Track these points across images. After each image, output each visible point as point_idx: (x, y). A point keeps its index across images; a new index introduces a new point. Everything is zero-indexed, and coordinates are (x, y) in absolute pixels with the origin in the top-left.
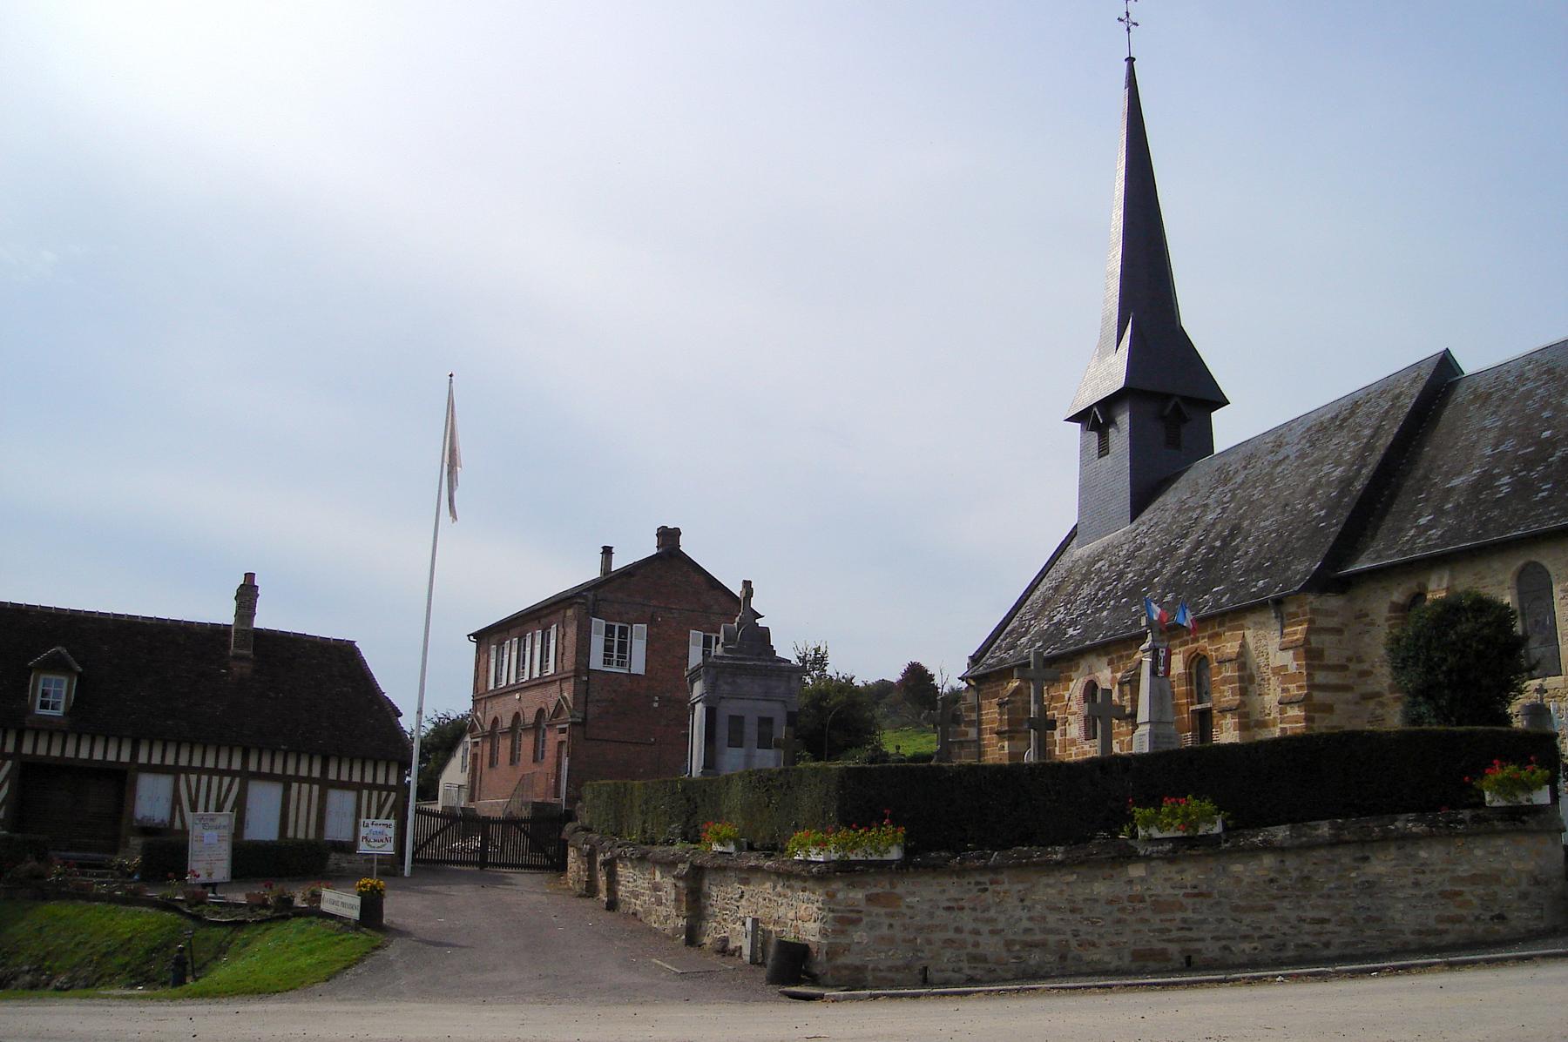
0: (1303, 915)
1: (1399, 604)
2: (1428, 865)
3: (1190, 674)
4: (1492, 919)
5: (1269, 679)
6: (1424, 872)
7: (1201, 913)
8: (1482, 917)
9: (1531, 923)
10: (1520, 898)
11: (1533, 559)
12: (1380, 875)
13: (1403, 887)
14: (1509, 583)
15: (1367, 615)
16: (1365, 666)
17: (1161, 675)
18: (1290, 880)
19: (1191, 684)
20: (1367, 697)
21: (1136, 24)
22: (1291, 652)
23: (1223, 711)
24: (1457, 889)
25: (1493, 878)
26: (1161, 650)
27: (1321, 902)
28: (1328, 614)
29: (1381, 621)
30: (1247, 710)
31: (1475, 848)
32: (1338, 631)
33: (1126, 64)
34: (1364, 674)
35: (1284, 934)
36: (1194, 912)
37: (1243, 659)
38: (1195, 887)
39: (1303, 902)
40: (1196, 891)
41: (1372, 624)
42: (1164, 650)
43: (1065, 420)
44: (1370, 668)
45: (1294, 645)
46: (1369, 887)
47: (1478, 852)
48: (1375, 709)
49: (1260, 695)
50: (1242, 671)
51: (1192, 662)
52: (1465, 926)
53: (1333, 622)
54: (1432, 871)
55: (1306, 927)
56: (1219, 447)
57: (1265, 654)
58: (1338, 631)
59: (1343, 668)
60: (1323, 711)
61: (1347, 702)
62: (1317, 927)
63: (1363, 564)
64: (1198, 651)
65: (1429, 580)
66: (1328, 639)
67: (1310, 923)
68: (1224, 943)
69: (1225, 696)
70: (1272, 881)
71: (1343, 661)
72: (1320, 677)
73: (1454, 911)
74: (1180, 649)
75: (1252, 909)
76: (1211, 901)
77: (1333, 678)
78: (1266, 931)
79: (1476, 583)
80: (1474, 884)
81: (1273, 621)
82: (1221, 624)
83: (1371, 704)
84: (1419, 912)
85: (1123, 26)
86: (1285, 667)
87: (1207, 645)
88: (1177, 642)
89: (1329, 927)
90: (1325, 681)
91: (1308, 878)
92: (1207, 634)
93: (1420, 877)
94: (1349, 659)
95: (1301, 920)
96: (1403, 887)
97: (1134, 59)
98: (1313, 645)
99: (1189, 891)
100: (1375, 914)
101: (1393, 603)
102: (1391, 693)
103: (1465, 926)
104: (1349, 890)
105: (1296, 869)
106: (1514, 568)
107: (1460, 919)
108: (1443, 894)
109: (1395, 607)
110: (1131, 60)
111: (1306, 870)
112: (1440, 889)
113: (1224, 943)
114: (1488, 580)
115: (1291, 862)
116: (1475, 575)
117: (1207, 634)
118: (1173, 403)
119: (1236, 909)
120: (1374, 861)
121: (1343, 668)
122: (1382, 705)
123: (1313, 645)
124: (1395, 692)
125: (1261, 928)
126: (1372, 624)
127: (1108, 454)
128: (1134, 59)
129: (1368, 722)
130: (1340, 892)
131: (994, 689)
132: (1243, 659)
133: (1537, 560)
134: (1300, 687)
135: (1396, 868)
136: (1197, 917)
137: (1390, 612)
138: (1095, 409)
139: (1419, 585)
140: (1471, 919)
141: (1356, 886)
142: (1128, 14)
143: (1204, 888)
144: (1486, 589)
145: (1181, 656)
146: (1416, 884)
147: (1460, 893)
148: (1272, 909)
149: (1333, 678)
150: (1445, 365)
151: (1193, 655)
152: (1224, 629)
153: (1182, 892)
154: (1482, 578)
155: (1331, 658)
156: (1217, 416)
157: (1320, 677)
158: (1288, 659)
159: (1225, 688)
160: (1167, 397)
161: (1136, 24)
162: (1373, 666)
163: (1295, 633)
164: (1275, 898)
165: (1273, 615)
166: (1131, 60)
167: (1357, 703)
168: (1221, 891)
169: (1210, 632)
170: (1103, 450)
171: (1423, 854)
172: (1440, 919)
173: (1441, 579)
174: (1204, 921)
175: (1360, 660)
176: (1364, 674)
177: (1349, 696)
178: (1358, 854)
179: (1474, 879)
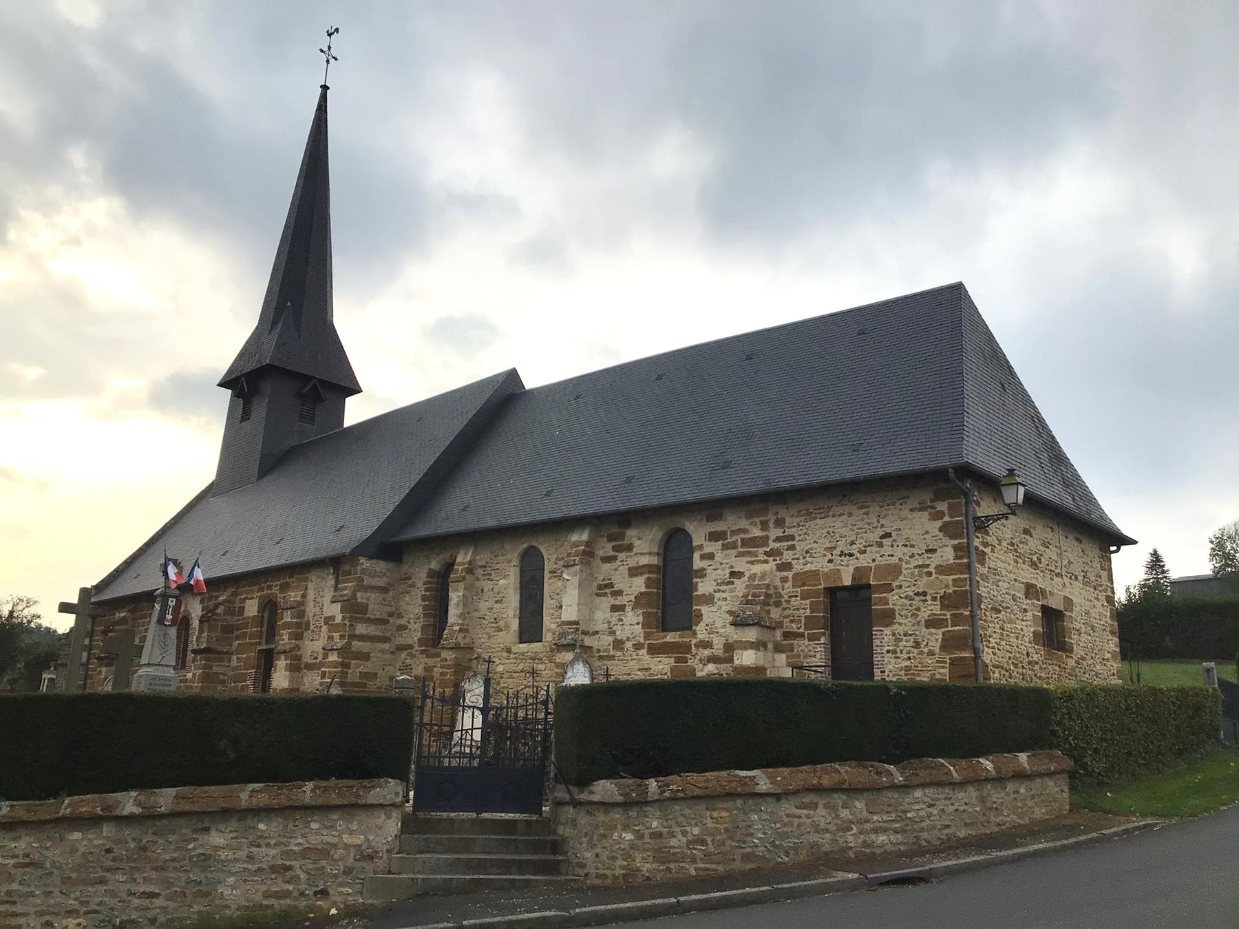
0: (133, 889)
1: (435, 571)
2: (265, 838)
3: (263, 617)
4: (316, 893)
5: (321, 627)
6: (259, 846)
7: (29, 885)
8: (307, 892)
9: (350, 899)
10: (345, 872)
11: (534, 544)
12: (217, 848)
13: (236, 860)
14: (516, 562)
15: (410, 578)
16: (403, 622)
17: (167, 623)
18: (127, 851)
19: (262, 627)
20: (401, 648)
21: (322, 51)
22: (340, 604)
23: (279, 653)
24: (288, 863)
25: (322, 852)
26: (170, 599)
27: (154, 875)
28: (374, 575)
29: (420, 584)
30: (299, 653)
31: (312, 821)
32: (384, 590)
33: (320, 90)
34: (403, 628)
35: (112, 909)
36: (20, 884)
37: (302, 608)
38: (27, 856)
39: (137, 875)
40: (28, 861)
41: (413, 586)
42: (174, 600)
43: (1134, 542)
44: (407, 624)
45: (342, 599)
46: (204, 861)
47: (314, 826)
48: (406, 659)
49: (312, 640)
50: (300, 618)
51: (264, 608)
52: (288, 901)
53: (381, 582)
54: (268, 845)
55: (136, 902)
56: (344, 427)
57: (321, 605)
58: (384, 590)
59: (385, 622)
60: (360, 659)
61: (382, 651)
62: (146, 902)
63: (422, 531)
64: (271, 597)
65: (458, 552)
66: (374, 597)
67: (139, 898)
68: (46, 918)
69: (283, 640)
70: (109, 851)
71: (384, 616)
72: (361, 629)
73: (280, 885)
74: (258, 595)
75: (84, 882)
76: (40, 872)
77: (372, 630)
78: (93, 907)
79: (491, 559)
80: (304, 858)
81: (331, 577)
82: (291, 576)
83: (404, 655)
84: (249, 887)
85: (324, 57)
86: (333, 618)
87: (278, 592)
88: (256, 588)
89: (158, 902)
90: (365, 632)
91: (145, 849)
92: (279, 583)
93: (254, 850)
94: (391, 615)
95: (131, 894)
96: (236, 860)
97: (328, 88)
98: (359, 600)
99: (20, 860)
100: (205, 889)
101: (430, 569)
102: (419, 646)
103: (288, 901)
104: (184, 863)
105: (134, 840)
106: (520, 550)
107: (287, 894)
108: (273, 869)
109: (432, 574)
110: (325, 88)
111: (144, 841)
112: (272, 863)
113: (46, 918)
114: (500, 558)
115: (128, 832)
116: (492, 552)
117: (279, 583)
118: (311, 384)
119: (65, 880)
120: (213, 832)
121: (385, 622)
122: (413, 656)
123: (359, 600)
124: (422, 646)
125: (88, 902)
126: (413, 586)
127: (249, 419)
128: (328, 88)
129: (400, 670)
130: (175, 864)
131: (107, 618)
132: (302, 608)
133: (537, 545)
134: (342, 637)
135: (233, 841)
136: (24, 889)
137: (427, 577)
138: (243, 379)
139: (451, 556)
140: (296, 894)
141: (191, 858)
142: (329, 48)
143: (36, 856)
144: (709, 564)
145: (257, 601)
146: (250, 858)
147: (290, 868)
148: (103, 881)
149: (372, 630)
150: (513, 375)
151: (266, 600)
152: (292, 579)
153: (12, 862)
154: (496, 556)
155: (375, 611)
156: (350, 402)
157: (361, 629)
158: (335, 611)
159: (285, 632)
160: (309, 378)
161: (322, 51)
162: (409, 622)
163: (345, 588)
164: (108, 870)
165: (332, 571)
166: (325, 88)
167: (392, 653)
168: (54, 862)
169: (281, 581)
170: (246, 416)
171: (262, 826)
172: (267, 895)
173: (466, 554)
174: (31, 894)
175: (400, 616)
176: (403, 628)
177: (386, 646)
178: (200, 826)
179: (305, 853)
